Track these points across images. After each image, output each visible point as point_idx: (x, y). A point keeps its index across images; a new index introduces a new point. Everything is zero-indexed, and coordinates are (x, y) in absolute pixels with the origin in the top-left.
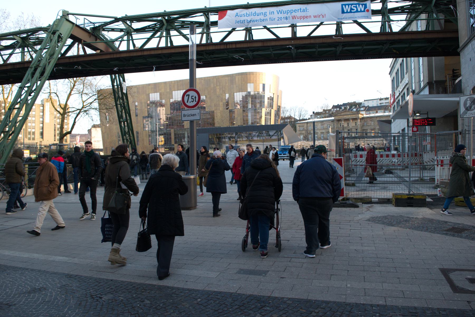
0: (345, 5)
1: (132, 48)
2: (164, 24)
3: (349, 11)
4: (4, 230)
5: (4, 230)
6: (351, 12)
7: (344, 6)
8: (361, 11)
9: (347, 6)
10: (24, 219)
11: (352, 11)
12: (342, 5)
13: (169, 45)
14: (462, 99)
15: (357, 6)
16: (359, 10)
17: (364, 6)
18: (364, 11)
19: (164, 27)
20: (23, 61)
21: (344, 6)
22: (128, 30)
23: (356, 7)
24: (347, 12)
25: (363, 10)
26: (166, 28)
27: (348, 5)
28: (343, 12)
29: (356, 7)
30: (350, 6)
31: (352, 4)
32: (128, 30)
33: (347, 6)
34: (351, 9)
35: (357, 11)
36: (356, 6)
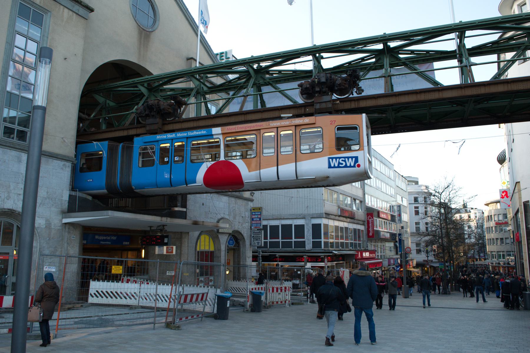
0: (332, 158)
1: (204, 114)
2: (251, 77)
3: (336, 165)
4: (139, 313)
5: (139, 313)
6: (338, 167)
7: (331, 160)
8: (350, 166)
9: (334, 160)
10: (448, 307)
11: (340, 165)
12: (329, 158)
13: (259, 107)
14: (502, 259)
15: (346, 159)
16: (348, 165)
17: (354, 159)
18: (354, 166)
19: (252, 82)
20: (41, 338)
21: (331, 160)
22: (198, 87)
23: (345, 161)
24: (334, 167)
25: (352, 165)
26: (254, 82)
27: (336, 158)
28: (330, 167)
29: (345, 161)
30: (338, 159)
31: (340, 158)
32: (198, 89)
33: (334, 160)
34: (339, 163)
35: (346, 166)
36: (345, 160)
